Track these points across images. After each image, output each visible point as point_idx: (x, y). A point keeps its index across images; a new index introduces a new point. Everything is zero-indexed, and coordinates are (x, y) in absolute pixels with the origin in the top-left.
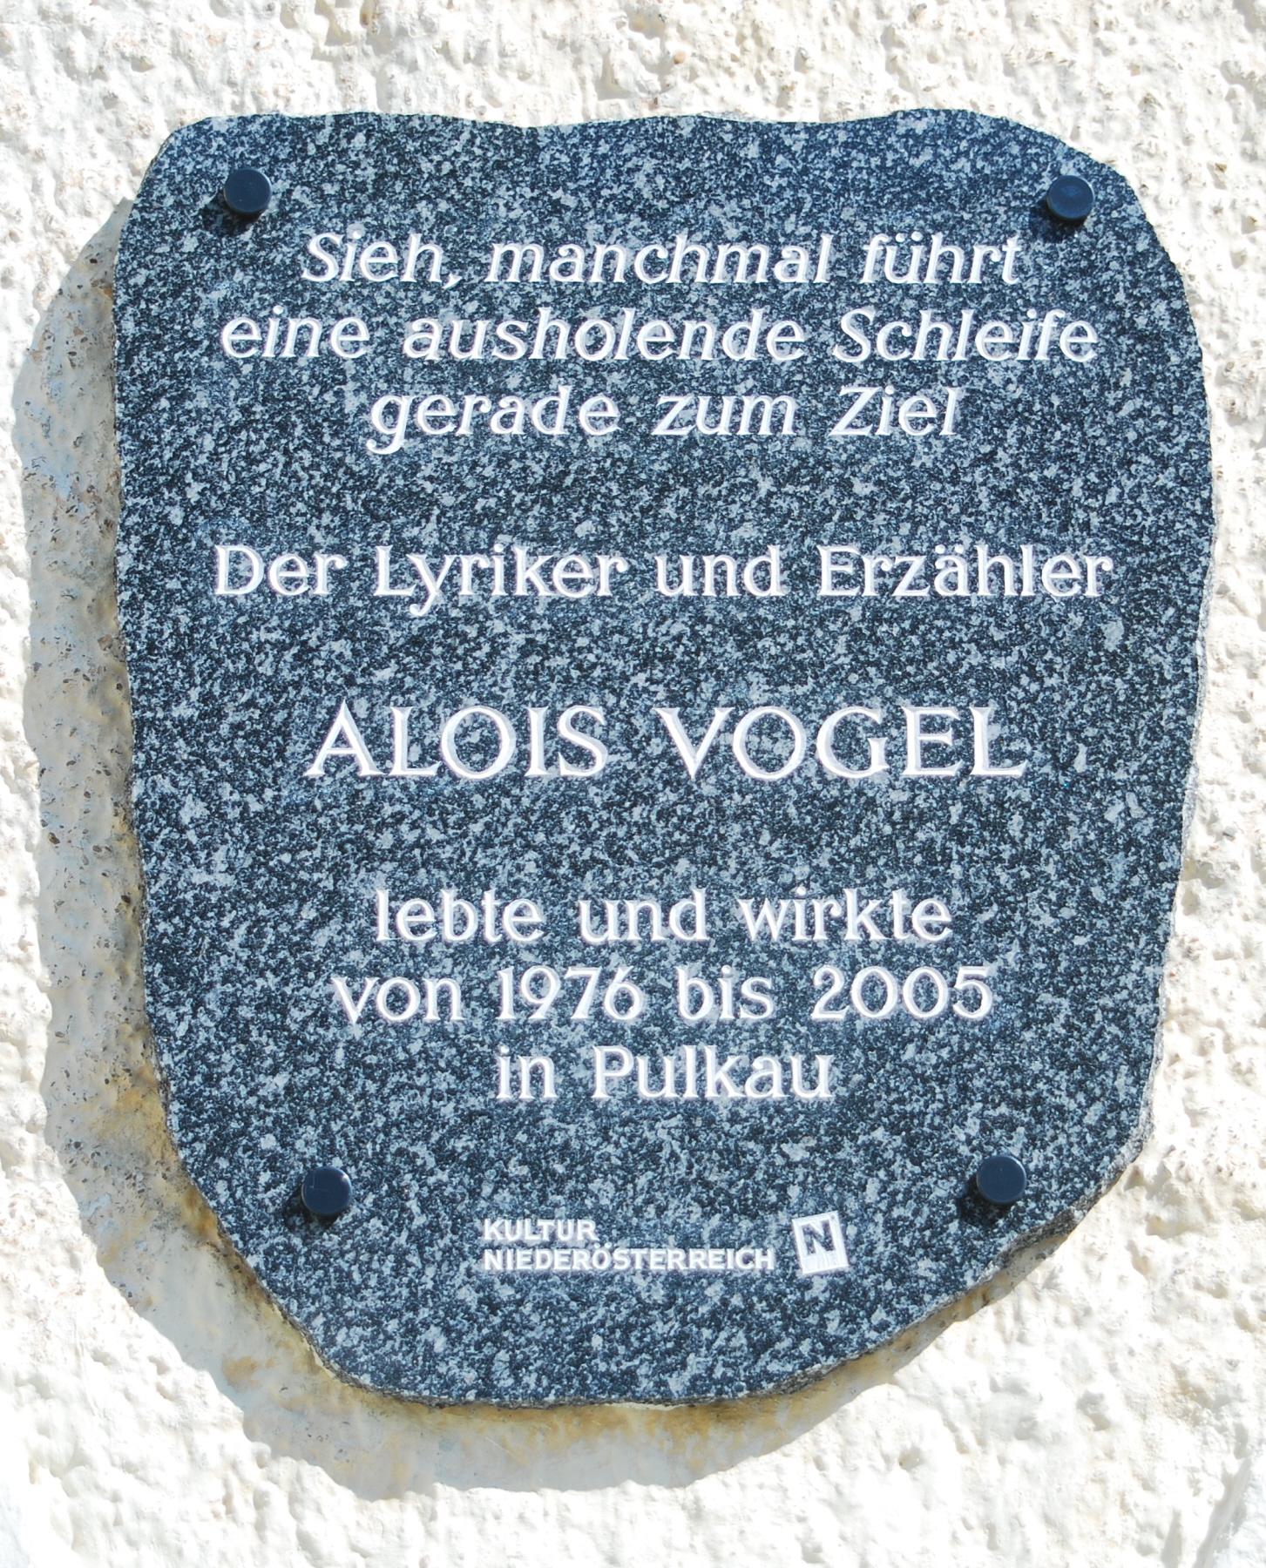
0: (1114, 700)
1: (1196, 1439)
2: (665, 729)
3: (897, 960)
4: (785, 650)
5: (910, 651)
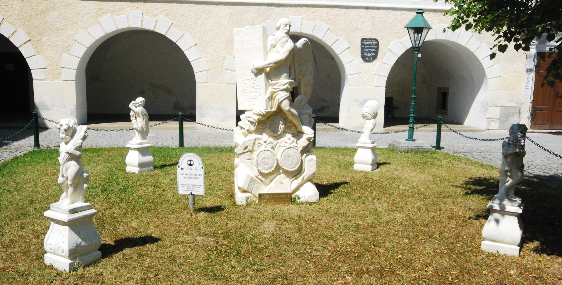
0: (377, 49)
1: (458, 183)
2: (346, 149)
3: (373, 54)
4: (372, 48)
5: (374, 48)
